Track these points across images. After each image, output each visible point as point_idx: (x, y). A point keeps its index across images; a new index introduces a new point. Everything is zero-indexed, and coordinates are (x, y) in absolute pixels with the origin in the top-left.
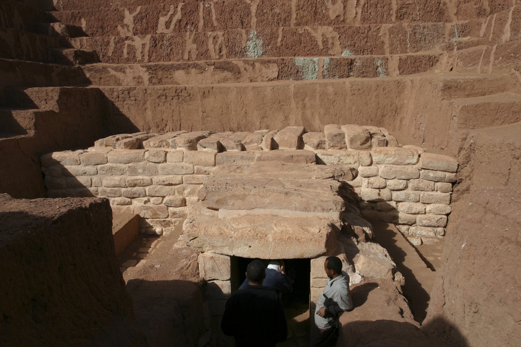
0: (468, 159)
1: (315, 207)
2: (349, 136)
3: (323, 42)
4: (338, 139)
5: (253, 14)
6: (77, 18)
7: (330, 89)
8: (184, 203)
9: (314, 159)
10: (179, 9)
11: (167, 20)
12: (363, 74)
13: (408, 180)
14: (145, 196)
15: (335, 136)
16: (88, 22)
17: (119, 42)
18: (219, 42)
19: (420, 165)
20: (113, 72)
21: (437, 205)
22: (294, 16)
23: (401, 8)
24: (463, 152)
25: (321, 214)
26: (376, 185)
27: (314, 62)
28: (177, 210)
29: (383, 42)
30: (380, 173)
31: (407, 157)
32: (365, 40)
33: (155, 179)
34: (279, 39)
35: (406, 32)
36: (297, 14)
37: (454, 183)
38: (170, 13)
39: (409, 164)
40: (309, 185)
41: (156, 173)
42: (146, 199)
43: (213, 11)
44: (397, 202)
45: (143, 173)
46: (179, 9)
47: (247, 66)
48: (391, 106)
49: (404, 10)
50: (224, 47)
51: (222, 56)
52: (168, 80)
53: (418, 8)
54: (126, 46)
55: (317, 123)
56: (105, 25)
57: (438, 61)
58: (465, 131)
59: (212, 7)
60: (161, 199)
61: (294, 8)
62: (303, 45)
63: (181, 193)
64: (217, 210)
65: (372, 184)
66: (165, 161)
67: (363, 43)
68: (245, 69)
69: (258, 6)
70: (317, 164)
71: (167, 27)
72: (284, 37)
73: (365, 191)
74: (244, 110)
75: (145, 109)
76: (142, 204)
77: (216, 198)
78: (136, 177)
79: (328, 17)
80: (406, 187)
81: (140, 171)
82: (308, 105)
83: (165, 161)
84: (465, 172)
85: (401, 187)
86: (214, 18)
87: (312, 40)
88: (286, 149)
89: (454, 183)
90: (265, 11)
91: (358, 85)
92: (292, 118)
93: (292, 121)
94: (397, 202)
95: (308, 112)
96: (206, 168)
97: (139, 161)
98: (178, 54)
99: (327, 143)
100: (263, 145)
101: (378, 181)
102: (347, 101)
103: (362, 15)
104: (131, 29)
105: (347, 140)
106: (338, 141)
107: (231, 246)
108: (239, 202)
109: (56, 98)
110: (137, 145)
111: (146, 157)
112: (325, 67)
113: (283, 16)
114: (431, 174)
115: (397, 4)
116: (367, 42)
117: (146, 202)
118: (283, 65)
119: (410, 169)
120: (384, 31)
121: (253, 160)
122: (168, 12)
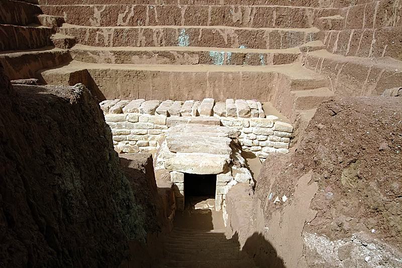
0: (298, 127)
1: (219, 153)
2: (239, 110)
3: (228, 40)
4: (233, 111)
5: (183, 16)
6: (61, 11)
7: (230, 76)
8: (148, 145)
9: (219, 123)
10: (132, 9)
11: (124, 16)
12: (251, 64)
13: (268, 136)
14: (126, 140)
15: (232, 109)
16: (68, 14)
17: (92, 32)
18: (161, 36)
19: (274, 128)
20: (91, 55)
21: (282, 149)
22: (210, 19)
23: (279, 18)
24: (296, 122)
25: (222, 156)
26: (251, 138)
27: (222, 54)
28: (144, 148)
29: (265, 42)
30: (253, 132)
31: (268, 124)
32: (255, 39)
33: (132, 131)
34: (200, 36)
35: (280, 36)
36: (212, 18)
37: (291, 138)
38: (126, 12)
39: (268, 127)
40: (217, 141)
41: (133, 128)
42: (127, 142)
43: (156, 12)
44: (262, 147)
45: (125, 128)
46: (132, 9)
47: (179, 55)
48: (266, 87)
49: (281, 19)
50: (164, 39)
51: (163, 45)
52: (127, 62)
53: (289, 18)
54: (97, 35)
55: (222, 96)
56: (81, 17)
57: (297, 58)
58: (298, 111)
59: (155, 9)
60: (135, 142)
61: (209, 14)
62: (215, 41)
63: (146, 139)
64: (176, 153)
65: (249, 137)
66: (138, 121)
67: (253, 42)
68: (178, 57)
69: (186, 10)
70: (221, 126)
71: (124, 21)
72: (202, 35)
73: (245, 140)
74: (178, 86)
75: (117, 83)
76: (125, 145)
77: (176, 147)
78: (121, 130)
79: (232, 21)
80: (267, 139)
81: (124, 126)
82: (217, 85)
83: (138, 121)
84: (296, 132)
85: (264, 139)
86: (156, 17)
87: (221, 38)
88: (205, 116)
89: (291, 138)
90: (190, 14)
91: (247, 74)
92: (207, 93)
93: (207, 95)
94: (262, 147)
95: (217, 90)
96: (160, 126)
97: (123, 121)
98: (133, 42)
99: (227, 113)
100: (192, 113)
101: (252, 136)
102: (240, 84)
103: (254, 21)
104: (99, 21)
105: (237, 112)
106: (233, 113)
107: (184, 169)
108: (186, 150)
109: (68, 80)
110: (120, 112)
111: (127, 119)
112: (228, 58)
113: (202, 18)
114: (279, 133)
115: (276, 15)
116: (255, 41)
117: (126, 144)
118: (202, 56)
119: (269, 130)
120: (267, 34)
121: (187, 123)
122: (125, 10)
